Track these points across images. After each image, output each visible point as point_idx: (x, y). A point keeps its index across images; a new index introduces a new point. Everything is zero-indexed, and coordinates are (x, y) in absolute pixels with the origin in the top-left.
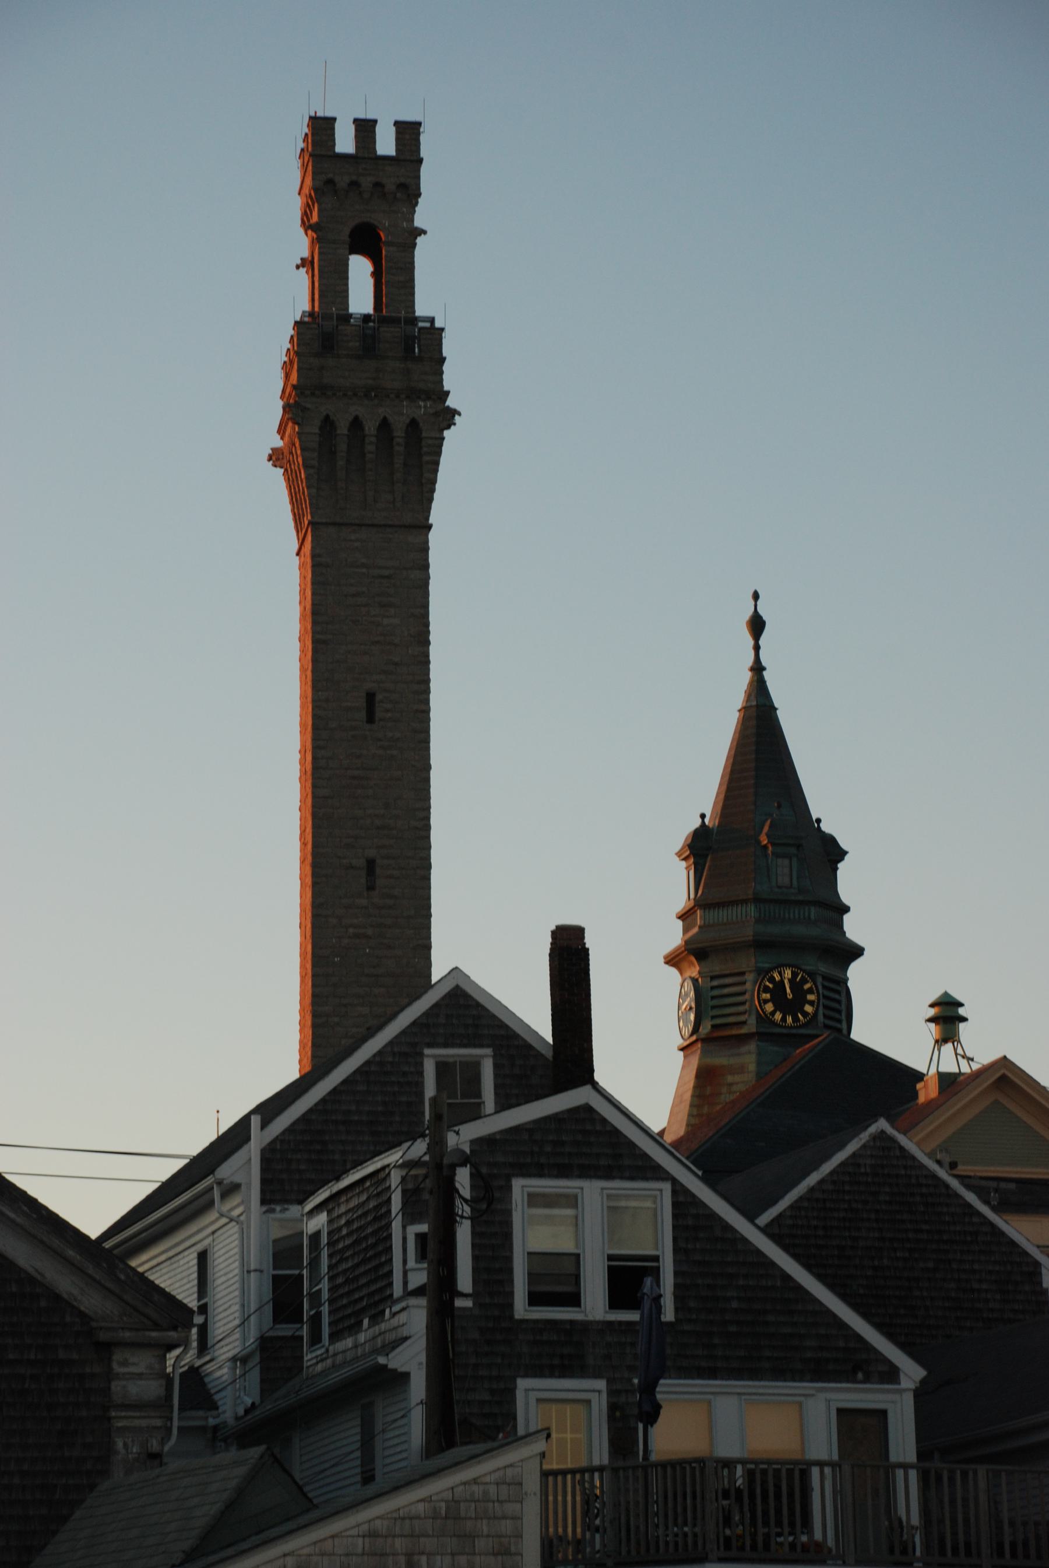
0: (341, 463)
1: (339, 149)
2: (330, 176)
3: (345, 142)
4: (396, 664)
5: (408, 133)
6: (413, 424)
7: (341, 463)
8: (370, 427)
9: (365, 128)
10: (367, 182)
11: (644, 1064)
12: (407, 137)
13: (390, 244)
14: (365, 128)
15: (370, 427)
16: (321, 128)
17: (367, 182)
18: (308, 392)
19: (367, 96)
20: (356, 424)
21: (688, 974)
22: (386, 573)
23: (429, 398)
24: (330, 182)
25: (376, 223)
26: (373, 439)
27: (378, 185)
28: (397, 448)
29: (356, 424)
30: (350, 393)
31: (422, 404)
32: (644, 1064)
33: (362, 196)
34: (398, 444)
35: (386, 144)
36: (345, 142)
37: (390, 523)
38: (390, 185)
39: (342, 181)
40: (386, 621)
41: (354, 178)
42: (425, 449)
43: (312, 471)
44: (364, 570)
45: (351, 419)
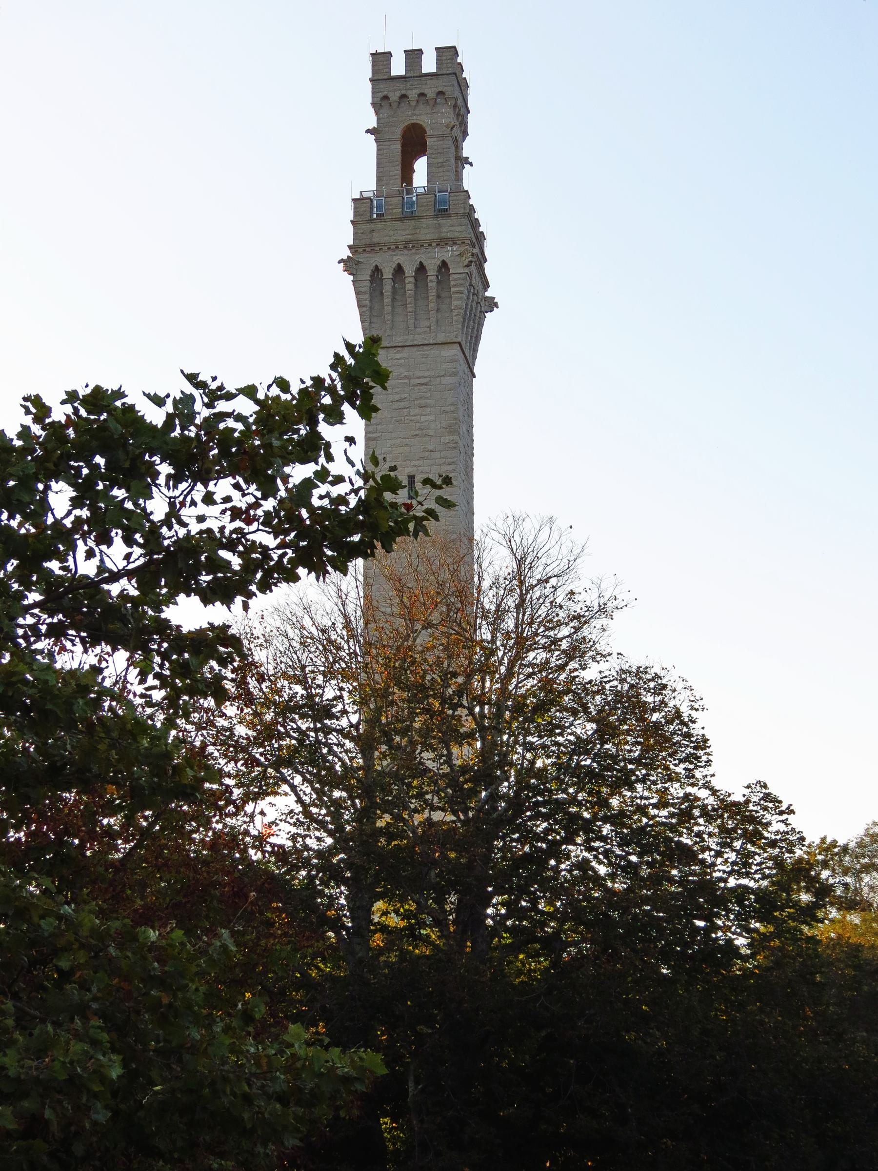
0: (387, 301)
1: (394, 73)
2: (385, 93)
3: (398, 68)
4: (432, 451)
5: (448, 55)
6: (444, 264)
7: (387, 301)
8: (410, 271)
9: (414, 56)
10: (413, 94)
11: (26, 602)
12: (445, 58)
13: (432, 136)
14: (414, 56)
15: (410, 271)
16: (381, 60)
17: (413, 94)
18: (361, 250)
19: (414, 32)
20: (399, 270)
21: (77, 512)
22: (422, 381)
23: (455, 244)
24: (386, 98)
25: (418, 122)
26: (412, 280)
27: (422, 95)
28: (430, 284)
29: (399, 270)
30: (392, 247)
31: (450, 248)
32: (26, 602)
33: (420, 110)
34: (431, 281)
35: (429, 65)
36: (398, 68)
37: (427, 342)
38: (431, 93)
39: (394, 96)
40: (423, 418)
41: (403, 92)
42: (452, 283)
43: (364, 309)
44: (406, 381)
45: (394, 266)
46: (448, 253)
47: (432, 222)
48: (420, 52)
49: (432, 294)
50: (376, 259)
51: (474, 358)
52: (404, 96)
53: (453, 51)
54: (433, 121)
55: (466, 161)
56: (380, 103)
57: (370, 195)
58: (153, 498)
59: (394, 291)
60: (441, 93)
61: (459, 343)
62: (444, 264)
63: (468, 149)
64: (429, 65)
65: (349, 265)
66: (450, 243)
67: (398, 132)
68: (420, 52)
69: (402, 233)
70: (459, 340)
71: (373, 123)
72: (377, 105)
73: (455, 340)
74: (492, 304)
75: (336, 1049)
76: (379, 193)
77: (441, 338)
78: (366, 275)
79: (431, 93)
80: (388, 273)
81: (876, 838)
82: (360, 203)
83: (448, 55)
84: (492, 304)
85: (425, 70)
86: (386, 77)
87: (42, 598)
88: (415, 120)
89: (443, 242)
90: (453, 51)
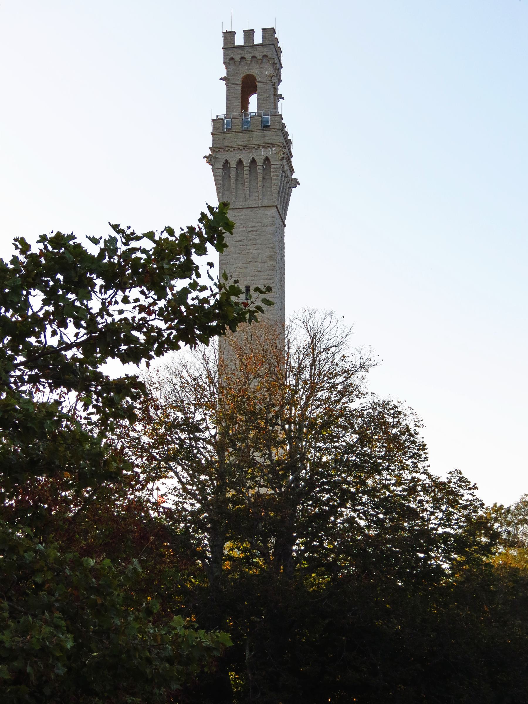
0: (233, 181)
1: (237, 44)
2: (232, 56)
3: (239, 41)
4: (260, 271)
5: (269, 33)
6: (267, 159)
7: (233, 181)
8: (246, 163)
9: (249, 34)
10: (248, 57)
11: (15, 362)
12: (267, 35)
13: (260, 82)
14: (249, 34)
15: (246, 163)
16: (229, 36)
17: (248, 57)
18: (217, 150)
19: (249, 19)
20: (240, 162)
21: (46, 308)
22: (254, 229)
23: (273, 146)
24: (232, 59)
25: (252, 73)
26: (248, 168)
27: (254, 57)
28: (259, 171)
29: (240, 162)
30: (236, 148)
31: (270, 149)
32: (15, 362)
33: (253, 66)
34: (259, 169)
35: (258, 39)
36: (239, 41)
37: (257, 206)
38: (259, 56)
39: (237, 58)
40: (254, 252)
41: (243, 55)
42: (272, 170)
43: (219, 186)
44: (244, 229)
45: (237, 160)
46: (270, 152)
47: (260, 133)
48: (252, 31)
49: (260, 177)
50: (226, 156)
51: (285, 215)
52: (243, 58)
53: (272, 31)
54: (260, 73)
55: (280, 97)
56: (228, 62)
57: (223, 117)
58: (92, 299)
59: (237, 175)
60: (265, 56)
61: (276, 206)
62: (267, 159)
63: (282, 89)
64: (258, 39)
65: (210, 159)
66: (271, 146)
67: (239, 79)
68: (252, 31)
69: (242, 140)
70: (276, 204)
71: (224, 74)
72: (227, 63)
73: (274, 204)
74: (296, 183)
75: (202, 631)
76: (228, 116)
77: (265, 203)
78: (220, 166)
79: (259, 56)
80: (233, 164)
81: (527, 504)
82: (216, 122)
83: (269, 33)
84: (296, 183)
85: (255, 42)
86: (232, 46)
87: (26, 359)
88: (249, 72)
89: (266, 146)
90: (272, 31)
